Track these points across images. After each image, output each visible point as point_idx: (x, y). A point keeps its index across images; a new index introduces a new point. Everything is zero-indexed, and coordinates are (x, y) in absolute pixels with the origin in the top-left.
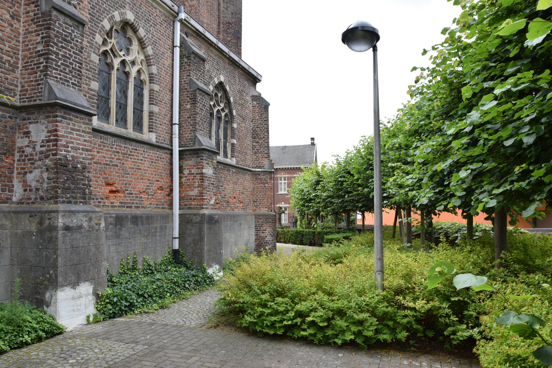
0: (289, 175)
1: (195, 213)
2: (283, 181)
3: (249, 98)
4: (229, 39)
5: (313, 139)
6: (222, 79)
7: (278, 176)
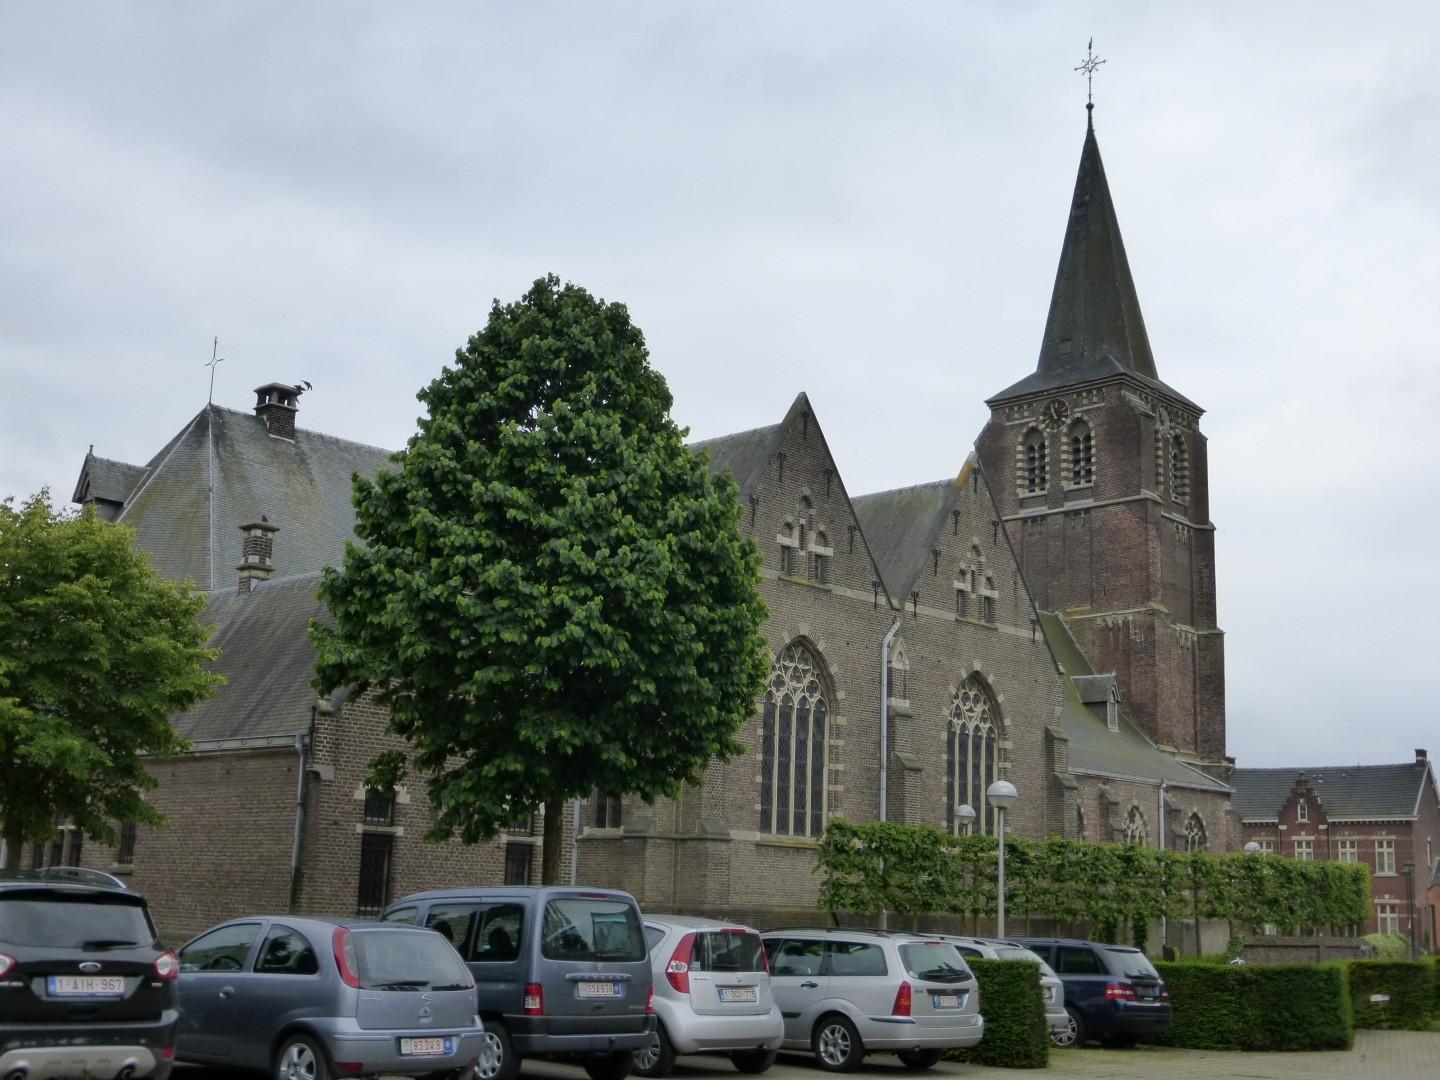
0: (1362, 838)
1: (864, 598)
2: (1348, 850)
3: (1222, 814)
4: (1208, 697)
5: (1421, 753)
6: (1195, 810)
7: (1337, 838)
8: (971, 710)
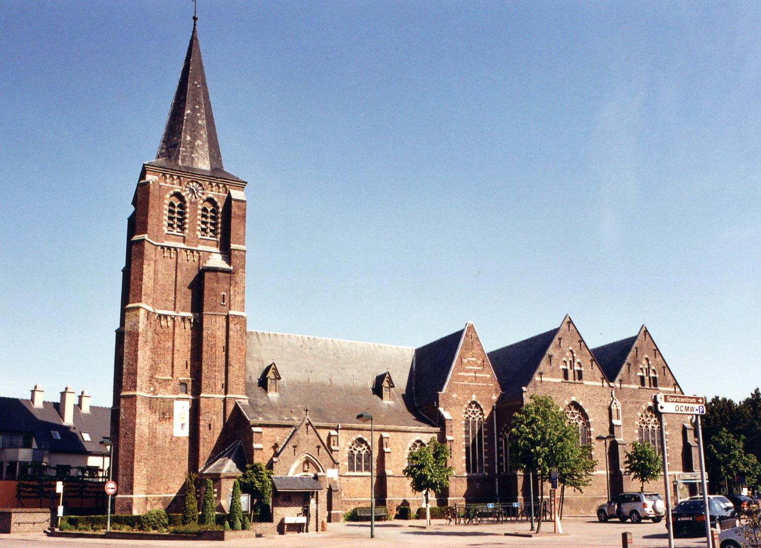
8: (649, 421)
